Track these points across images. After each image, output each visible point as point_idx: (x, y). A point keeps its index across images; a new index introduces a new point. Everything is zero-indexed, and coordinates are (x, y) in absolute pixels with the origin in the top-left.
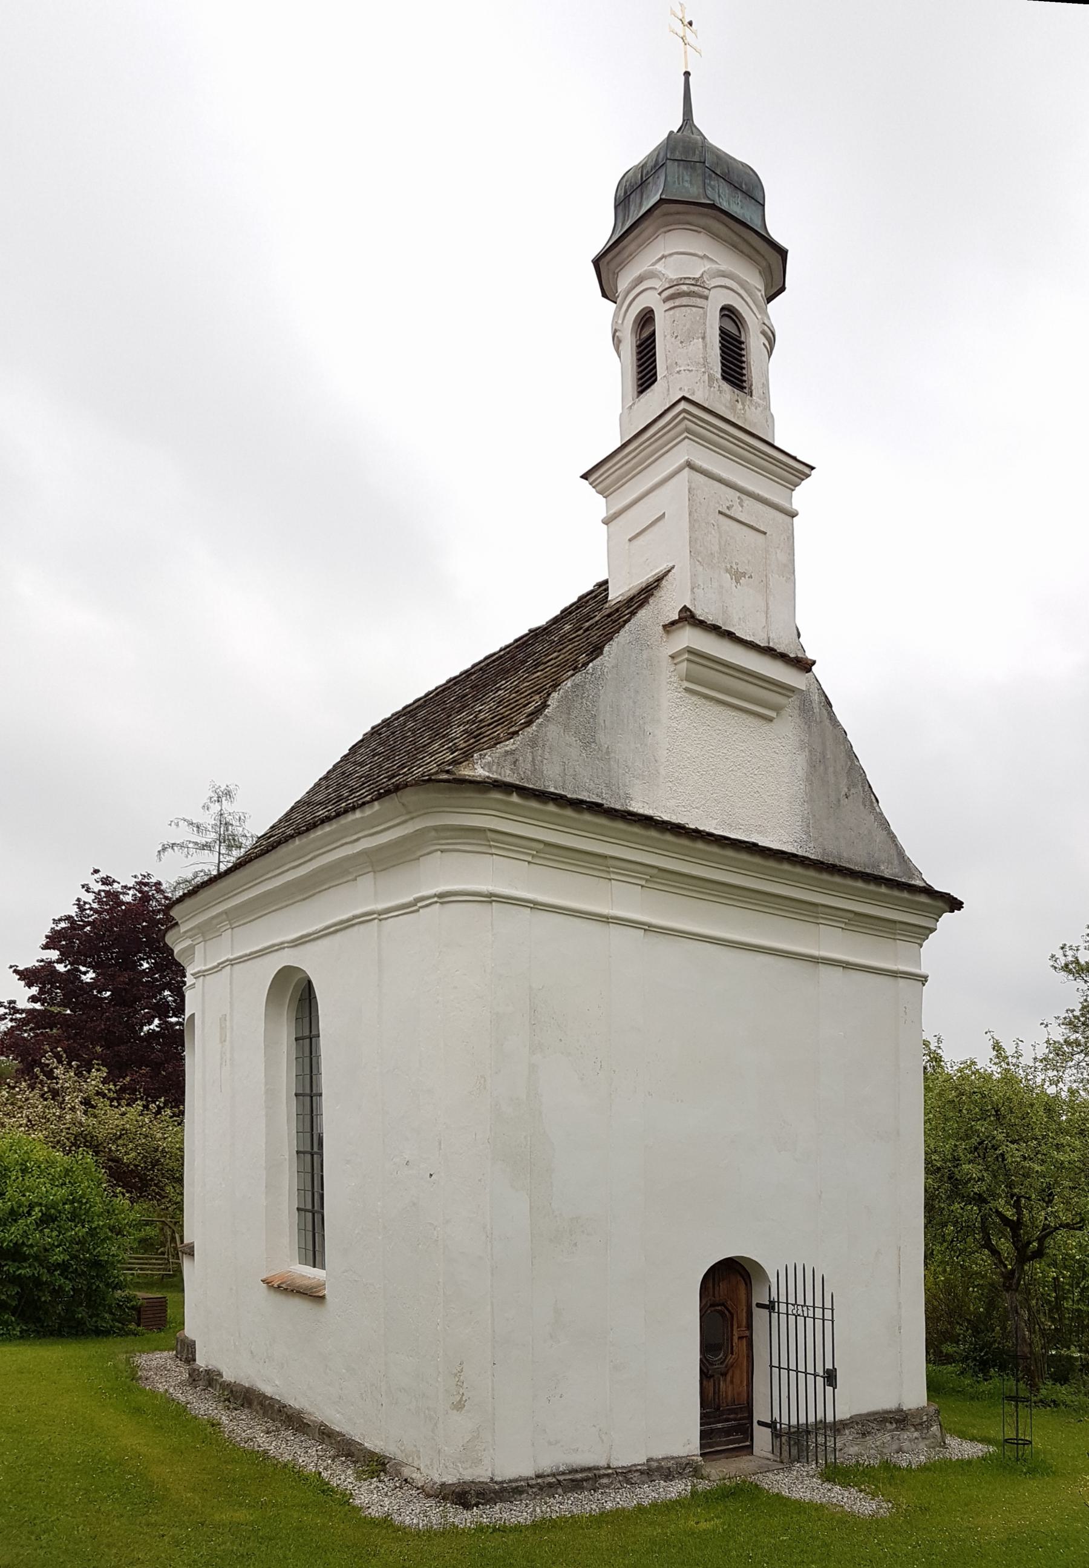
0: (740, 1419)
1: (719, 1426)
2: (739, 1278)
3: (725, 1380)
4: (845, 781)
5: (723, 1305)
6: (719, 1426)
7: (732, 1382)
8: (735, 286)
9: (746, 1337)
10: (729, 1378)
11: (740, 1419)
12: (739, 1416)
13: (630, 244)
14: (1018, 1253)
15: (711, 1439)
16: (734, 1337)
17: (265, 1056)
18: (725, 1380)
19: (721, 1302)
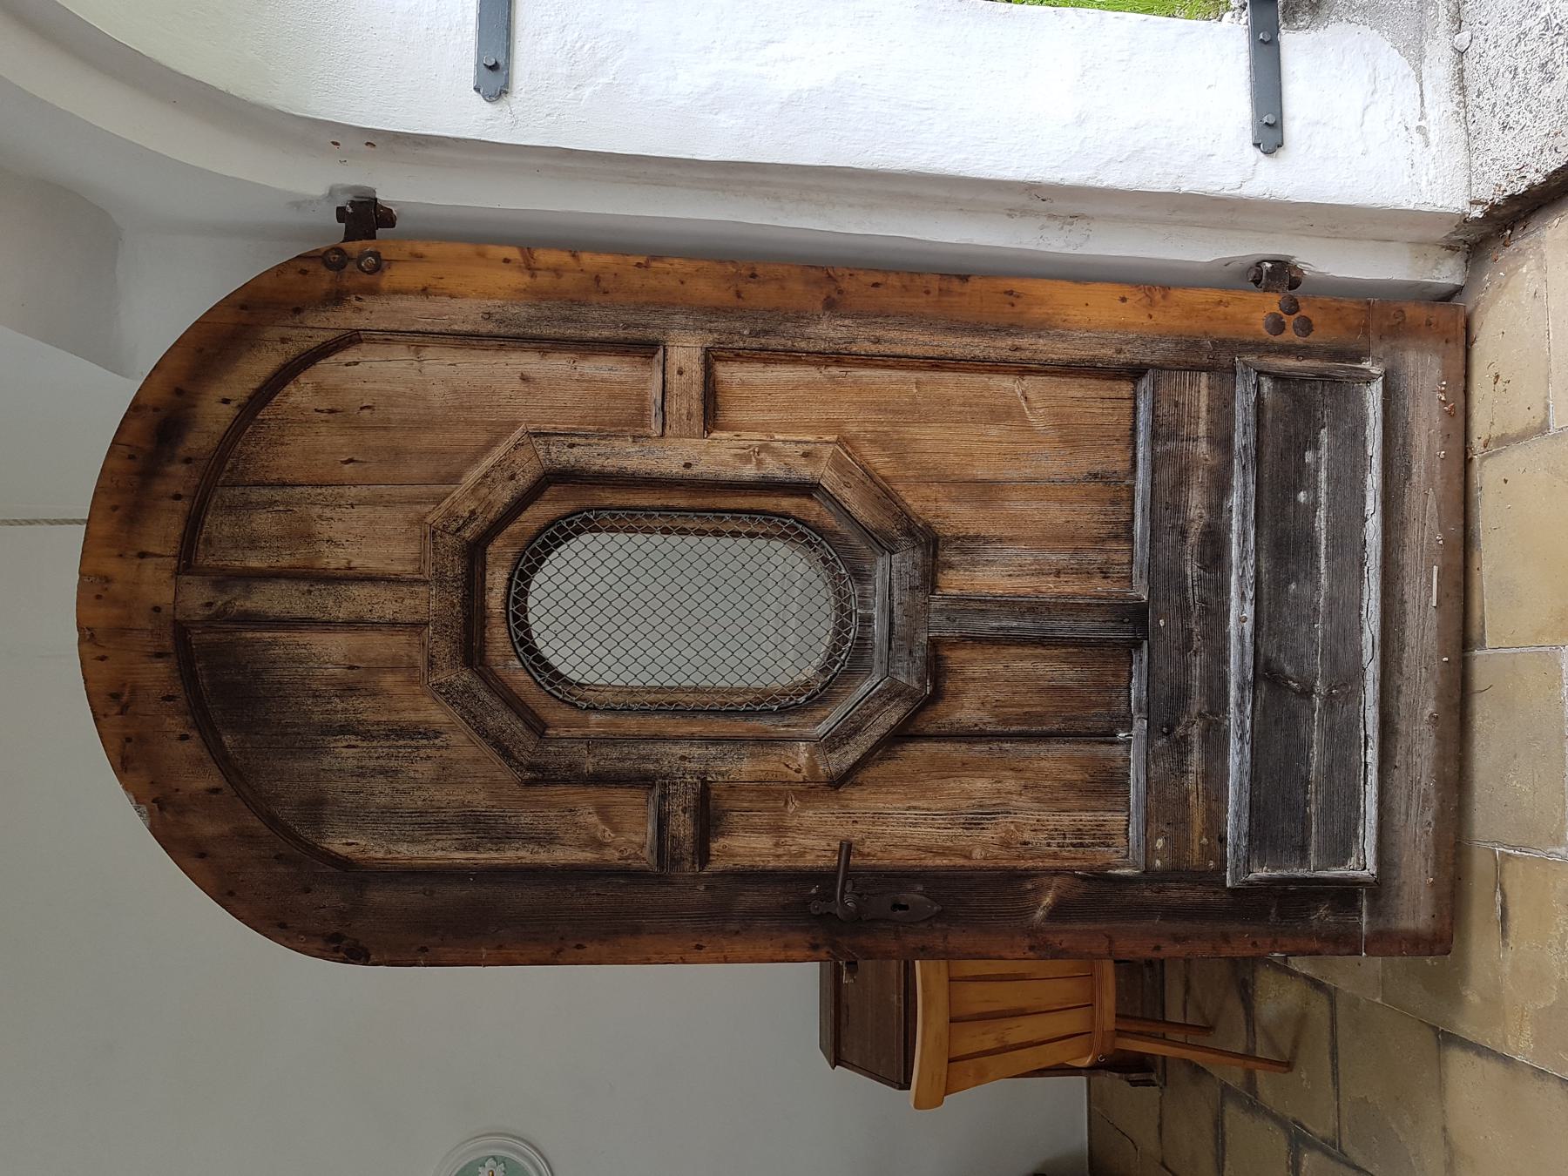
0: (1222, 442)
1: (1240, 614)
2: (300, 394)
3: (971, 545)
4: (1206, 1013)
5: (475, 554)
6: (1240, 614)
7: (986, 491)
8: (498, 635)
9: (710, 359)
10: (959, 516)
11: (1222, 442)
12: (1203, 448)
13: (1455, 530)
14: (186, 636)
15: (1307, 693)
16: (705, 467)
17: (354, 240)
18: (971, 545)
19: (456, 568)
